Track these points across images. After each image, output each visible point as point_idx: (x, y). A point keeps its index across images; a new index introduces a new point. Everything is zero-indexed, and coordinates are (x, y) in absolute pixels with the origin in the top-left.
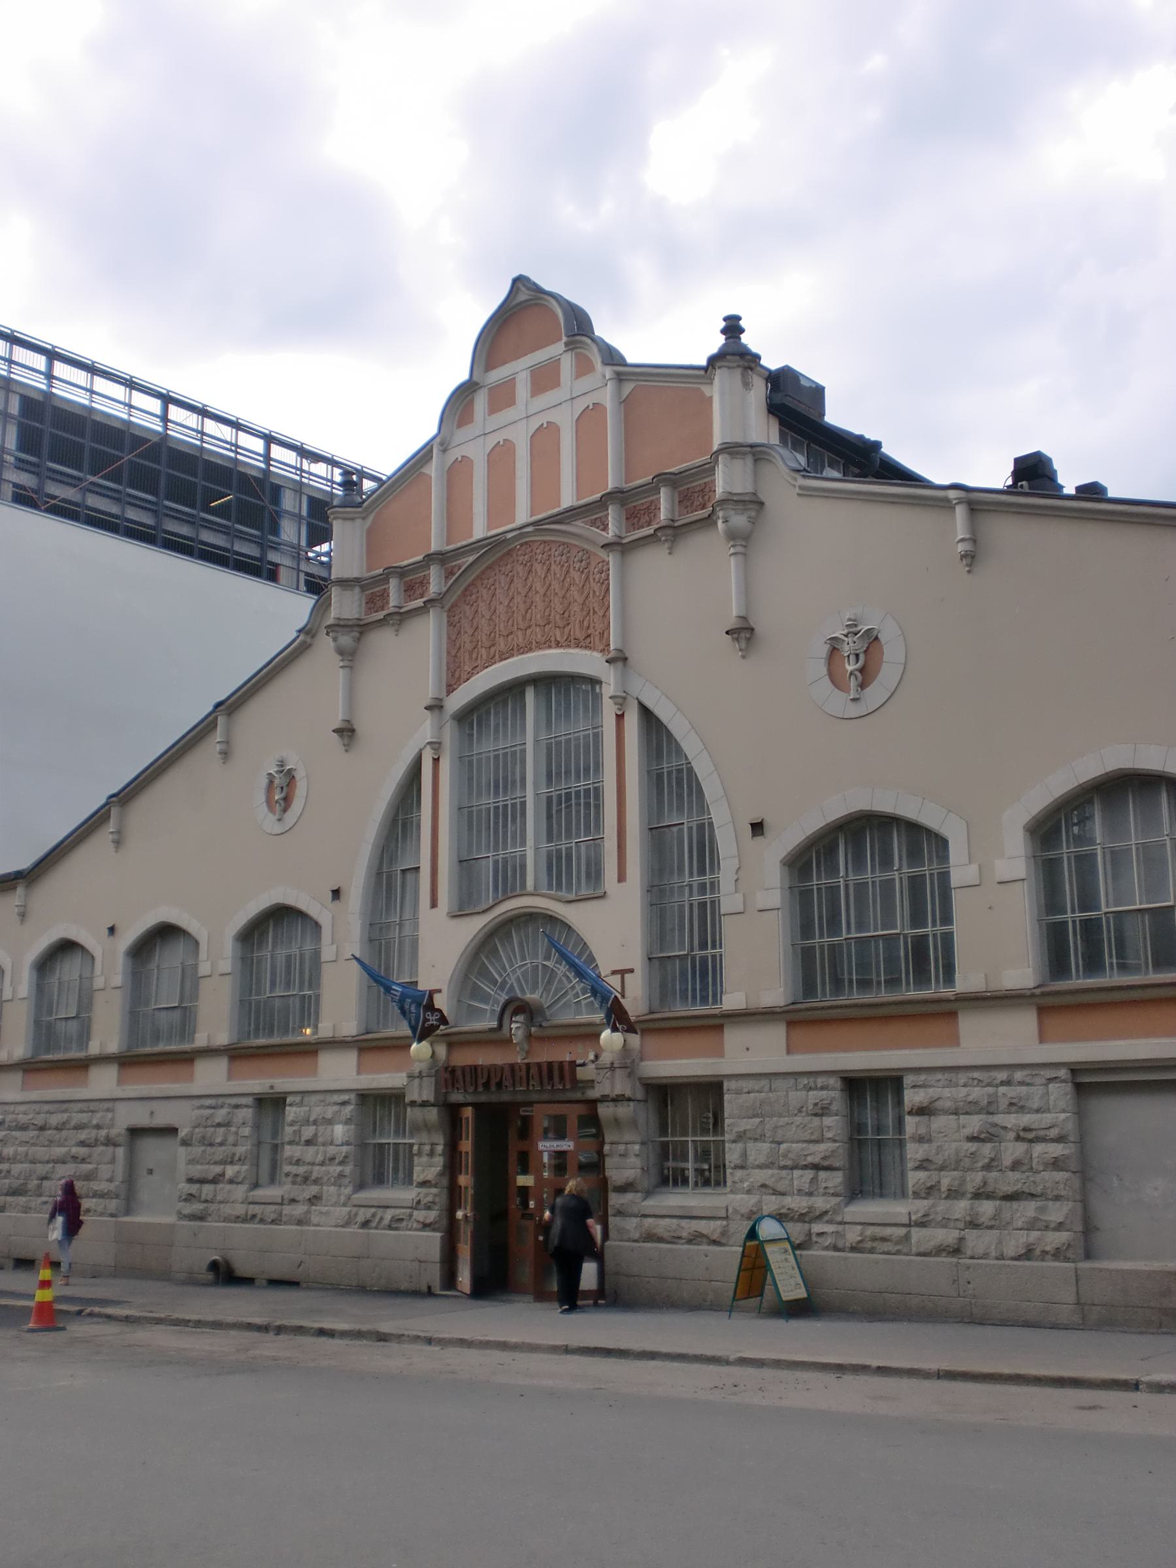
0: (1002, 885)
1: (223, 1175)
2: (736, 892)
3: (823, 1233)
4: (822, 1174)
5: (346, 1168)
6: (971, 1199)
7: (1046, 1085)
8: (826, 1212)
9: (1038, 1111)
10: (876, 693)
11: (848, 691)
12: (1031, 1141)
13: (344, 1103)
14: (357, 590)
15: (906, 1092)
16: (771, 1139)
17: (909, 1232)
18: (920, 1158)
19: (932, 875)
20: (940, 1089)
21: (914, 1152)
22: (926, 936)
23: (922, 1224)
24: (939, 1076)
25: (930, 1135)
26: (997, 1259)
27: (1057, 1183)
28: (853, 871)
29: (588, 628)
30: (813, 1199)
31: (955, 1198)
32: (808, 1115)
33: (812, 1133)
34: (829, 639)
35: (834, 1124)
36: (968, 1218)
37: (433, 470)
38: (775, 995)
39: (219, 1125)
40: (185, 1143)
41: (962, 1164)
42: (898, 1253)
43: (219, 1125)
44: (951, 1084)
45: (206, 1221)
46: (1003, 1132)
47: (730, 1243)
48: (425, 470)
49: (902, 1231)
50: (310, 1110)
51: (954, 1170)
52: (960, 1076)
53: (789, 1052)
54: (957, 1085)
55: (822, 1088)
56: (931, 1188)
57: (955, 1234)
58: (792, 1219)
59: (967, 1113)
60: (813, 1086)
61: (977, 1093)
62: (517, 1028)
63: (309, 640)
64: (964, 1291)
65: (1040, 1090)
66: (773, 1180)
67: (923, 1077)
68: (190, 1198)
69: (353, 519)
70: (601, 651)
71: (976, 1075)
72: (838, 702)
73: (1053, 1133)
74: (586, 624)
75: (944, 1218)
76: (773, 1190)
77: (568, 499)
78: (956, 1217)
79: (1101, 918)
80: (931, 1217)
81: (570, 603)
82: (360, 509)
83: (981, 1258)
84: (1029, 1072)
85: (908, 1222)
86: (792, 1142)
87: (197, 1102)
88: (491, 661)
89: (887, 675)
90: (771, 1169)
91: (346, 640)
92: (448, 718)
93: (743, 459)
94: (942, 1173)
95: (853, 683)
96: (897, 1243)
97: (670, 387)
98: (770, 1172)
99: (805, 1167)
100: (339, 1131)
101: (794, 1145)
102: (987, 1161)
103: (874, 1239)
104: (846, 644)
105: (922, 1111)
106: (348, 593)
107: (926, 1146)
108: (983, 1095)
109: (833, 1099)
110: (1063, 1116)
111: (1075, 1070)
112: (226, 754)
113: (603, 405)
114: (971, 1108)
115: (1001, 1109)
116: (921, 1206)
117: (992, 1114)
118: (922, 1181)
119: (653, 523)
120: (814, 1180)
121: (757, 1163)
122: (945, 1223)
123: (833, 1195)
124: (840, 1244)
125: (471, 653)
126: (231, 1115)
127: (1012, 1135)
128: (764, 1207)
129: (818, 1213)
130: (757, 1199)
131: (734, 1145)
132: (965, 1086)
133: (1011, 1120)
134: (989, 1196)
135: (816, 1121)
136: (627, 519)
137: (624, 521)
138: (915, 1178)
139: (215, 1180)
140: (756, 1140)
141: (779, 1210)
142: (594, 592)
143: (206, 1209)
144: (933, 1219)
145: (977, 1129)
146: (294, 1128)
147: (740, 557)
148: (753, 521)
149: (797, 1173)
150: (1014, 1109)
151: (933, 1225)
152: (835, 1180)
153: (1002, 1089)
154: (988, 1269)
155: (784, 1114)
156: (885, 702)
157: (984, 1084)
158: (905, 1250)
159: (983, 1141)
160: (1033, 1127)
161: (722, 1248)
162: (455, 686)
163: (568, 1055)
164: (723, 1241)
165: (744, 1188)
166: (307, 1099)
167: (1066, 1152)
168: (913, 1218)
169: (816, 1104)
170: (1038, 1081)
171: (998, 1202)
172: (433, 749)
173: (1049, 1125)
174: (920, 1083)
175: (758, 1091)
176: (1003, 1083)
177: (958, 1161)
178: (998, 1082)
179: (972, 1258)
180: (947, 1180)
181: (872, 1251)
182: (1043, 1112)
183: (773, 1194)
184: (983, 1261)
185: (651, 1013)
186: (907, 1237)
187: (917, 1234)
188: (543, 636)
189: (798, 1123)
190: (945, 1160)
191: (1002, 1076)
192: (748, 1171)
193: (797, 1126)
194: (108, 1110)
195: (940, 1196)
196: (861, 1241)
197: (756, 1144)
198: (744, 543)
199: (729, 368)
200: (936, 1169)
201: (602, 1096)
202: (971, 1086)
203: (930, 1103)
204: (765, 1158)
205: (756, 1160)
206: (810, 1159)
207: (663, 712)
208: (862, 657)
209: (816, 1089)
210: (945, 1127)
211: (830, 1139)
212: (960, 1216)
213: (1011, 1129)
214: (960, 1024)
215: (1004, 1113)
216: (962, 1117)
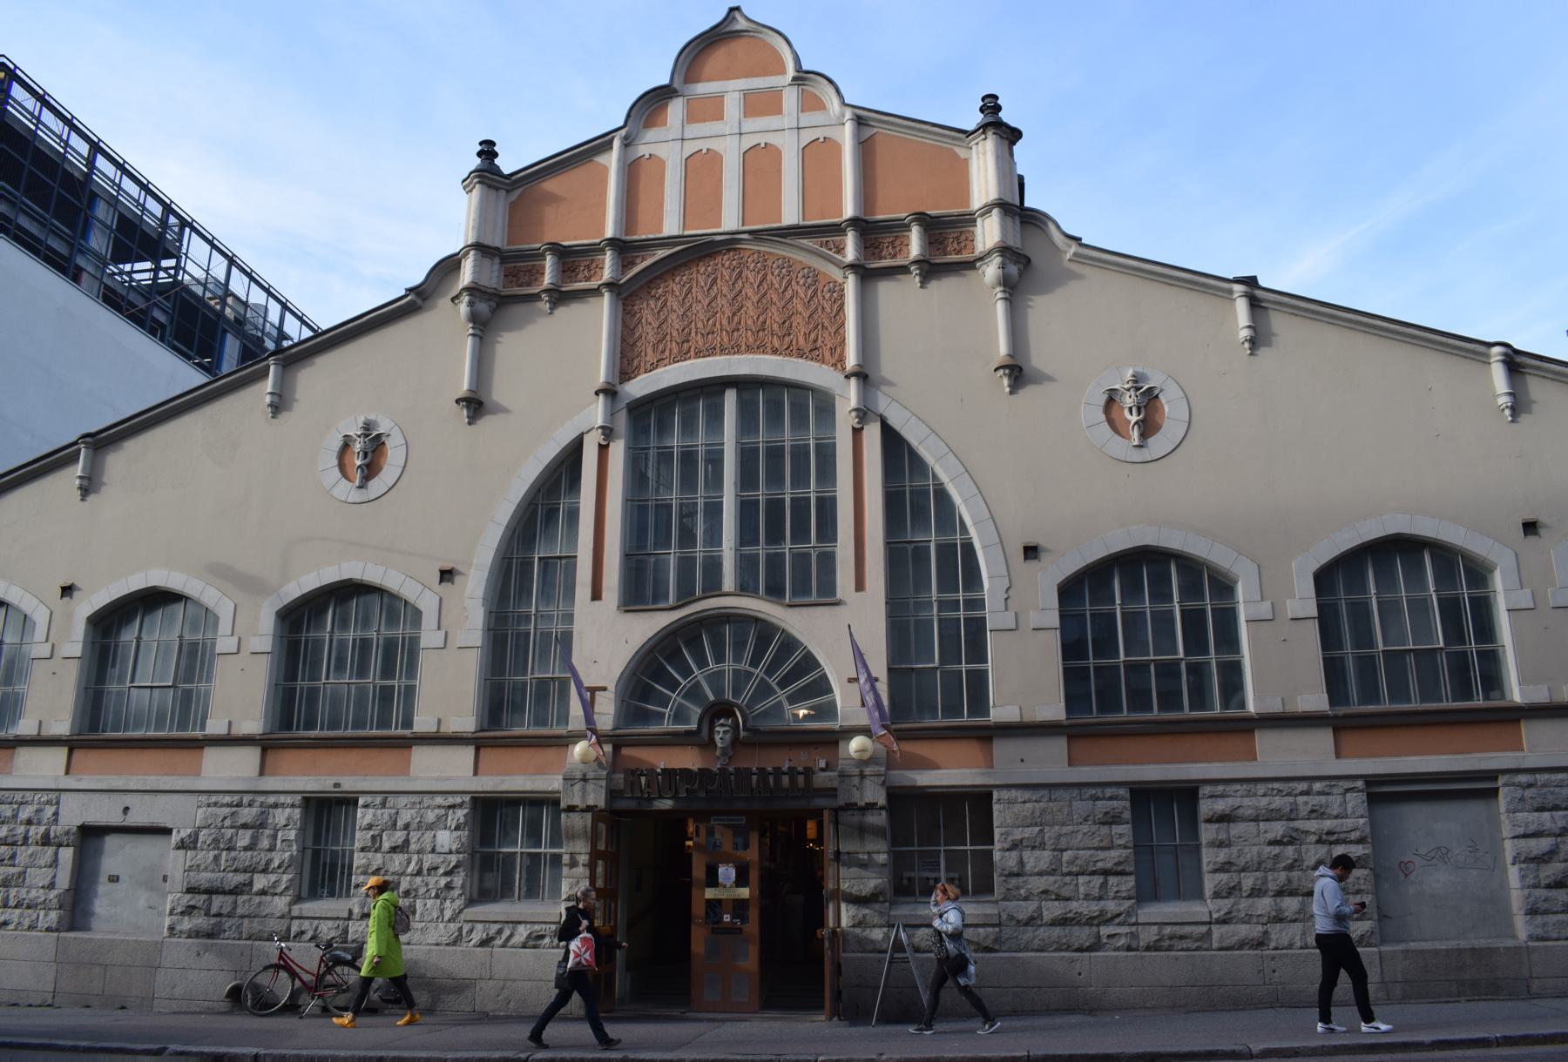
0: (1294, 621)
1: (251, 884)
2: (1262, 600)
3: (1115, 935)
4: (1112, 880)
5: (456, 879)
6: (1273, 896)
7: (1344, 794)
8: (1119, 915)
9: (1336, 817)
10: (377, 485)
11: (1127, 437)
12: (1331, 843)
13: (461, 806)
14: (497, 260)
15: (1201, 802)
16: (1053, 847)
17: (1210, 929)
18: (1222, 861)
19: (556, 632)
20: (1239, 799)
21: (1209, 857)
22: (191, 690)
23: (1223, 921)
24: (1238, 787)
25: (1230, 840)
26: (1301, 948)
27: (1358, 878)
28: (338, 626)
29: (815, 341)
30: (1102, 903)
31: (1258, 896)
32: (1094, 823)
33: (1102, 840)
34: (1109, 390)
35: (1123, 831)
36: (1273, 913)
37: (612, 161)
38: (253, 725)
39: (245, 826)
40: (182, 846)
41: (1264, 865)
42: (1197, 949)
43: (245, 826)
44: (1249, 794)
45: (218, 938)
46: (1303, 836)
47: (1003, 949)
48: (601, 159)
49: (1204, 929)
50: (397, 813)
51: (1256, 871)
52: (1259, 786)
53: (1070, 764)
54: (1255, 795)
55: (1111, 798)
56: (1234, 887)
57: (1260, 928)
58: (1079, 923)
59: (1267, 820)
60: (1101, 796)
61: (1278, 802)
62: (724, 732)
63: (419, 302)
64: (1270, 979)
65: (1339, 799)
66: (1057, 885)
67: (1221, 788)
68: (190, 910)
69: (497, 189)
70: (832, 366)
71: (1276, 785)
72: (346, 490)
73: (1354, 836)
74: (813, 336)
75: (1247, 915)
76: (1057, 895)
77: (790, 215)
78: (1259, 913)
79: (1119, 666)
80: (1233, 915)
81: (793, 313)
82: (508, 181)
83: (1286, 948)
84: (1328, 783)
85: (1208, 920)
86: (1078, 849)
87: (203, 798)
88: (684, 356)
89: (387, 476)
90: (1053, 875)
91: (483, 307)
92: (625, 405)
93: (492, 259)
94: (1243, 874)
95: (1135, 434)
96: (1197, 940)
97: (898, 137)
98: (1052, 878)
99: (1093, 873)
100: (445, 839)
101: (1081, 852)
102: (1289, 861)
103: (1171, 938)
104: (357, 442)
105: (1224, 818)
106: (487, 262)
107: (1226, 850)
108: (1285, 803)
109: (1125, 808)
110: (1362, 821)
111: (1371, 781)
112: (277, 407)
113: (835, 141)
114: (1272, 816)
115: (1300, 816)
116: (1225, 905)
117: (1293, 820)
118: (1223, 883)
119: (592, 279)
120: (1104, 885)
121: (1037, 870)
122: (1247, 920)
123: (1124, 898)
124: (1134, 945)
125: (655, 347)
126: (264, 816)
127: (1313, 838)
128: (1045, 913)
129: (1109, 916)
130: (1036, 905)
131: (1007, 853)
132: (1264, 795)
133: (1312, 825)
134: (1292, 894)
135: (1104, 830)
136: (505, 276)
137: (502, 277)
138: (1210, 883)
139: (236, 891)
140: (1033, 848)
141: (1066, 914)
142: (823, 308)
143: (219, 924)
144: (1235, 916)
145: (1281, 833)
146: (371, 833)
147: (478, 339)
148: (1021, 273)
149: (1081, 879)
150: (1314, 815)
151: (1234, 921)
152: (1129, 883)
153: (1301, 799)
154: (1294, 958)
155: (1068, 823)
156: (1170, 453)
157: (1284, 793)
158: (1206, 946)
159: (1286, 844)
160: (1336, 830)
161: (993, 955)
162: (633, 375)
163: (787, 761)
164: (997, 947)
165: (1021, 895)
166: (391, 800)
167: (1367, 852)
168: (1215, 916)
169: (1106, 813)
170: (1335, 791)
171: (1300, 898)
172: (603, 434)
173: (1350, 829)
174: (1219, 793)
175: (1036, 801)
176: (1302, 793)
177: (1260, 864)
178: (1298, 791)
179: (1276, 949)
180: (1248, 881)
181: (1170, 949)
182: (1342, 817)
183: (1056, 900)
184: (1289, 951)
185: (482, 731)
186: (1209, 933)
187: (1217, 931)
188: (755, 341)
189: (1085, 831)
190: (1247, 863)
191: (1303, 786)
192: (1025, 878)
193: (1084, 834)
194: (49, 802)
195: (1241, 895)
196: (1159, 940)
197: (1034, 852)
198: (482, 328)
199: (1001, 137)
200: (1235, 871)
201: (846, 804)
202: (1270, 795)
203: (1232, 811)
204: (1047, 865)
205: (1035, 867)
206: (1100, 865)
207: (913, 434)
208: (370, 455)
209: (1104, 799)
210: (1245, 832)
211: (1120, 845)
212: (1264, 911)
213: (1314, 833)
214: (413, 752)
215: (1304, 819)
216: (1261, 824)
